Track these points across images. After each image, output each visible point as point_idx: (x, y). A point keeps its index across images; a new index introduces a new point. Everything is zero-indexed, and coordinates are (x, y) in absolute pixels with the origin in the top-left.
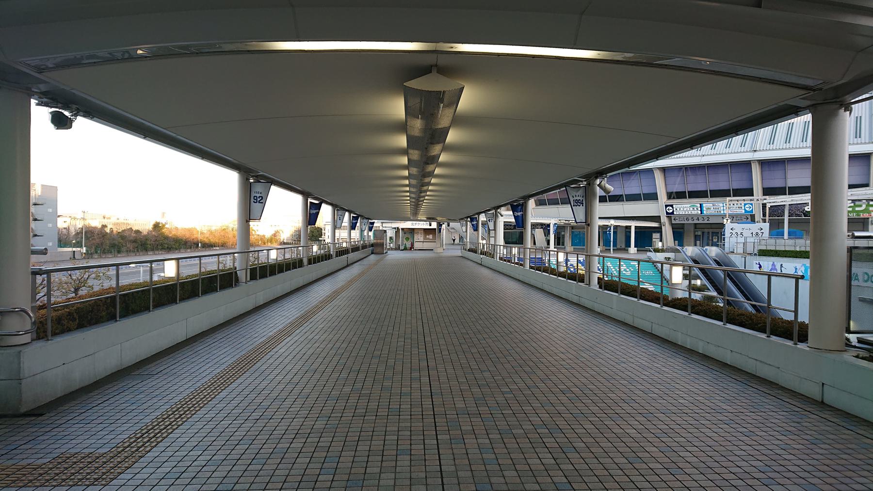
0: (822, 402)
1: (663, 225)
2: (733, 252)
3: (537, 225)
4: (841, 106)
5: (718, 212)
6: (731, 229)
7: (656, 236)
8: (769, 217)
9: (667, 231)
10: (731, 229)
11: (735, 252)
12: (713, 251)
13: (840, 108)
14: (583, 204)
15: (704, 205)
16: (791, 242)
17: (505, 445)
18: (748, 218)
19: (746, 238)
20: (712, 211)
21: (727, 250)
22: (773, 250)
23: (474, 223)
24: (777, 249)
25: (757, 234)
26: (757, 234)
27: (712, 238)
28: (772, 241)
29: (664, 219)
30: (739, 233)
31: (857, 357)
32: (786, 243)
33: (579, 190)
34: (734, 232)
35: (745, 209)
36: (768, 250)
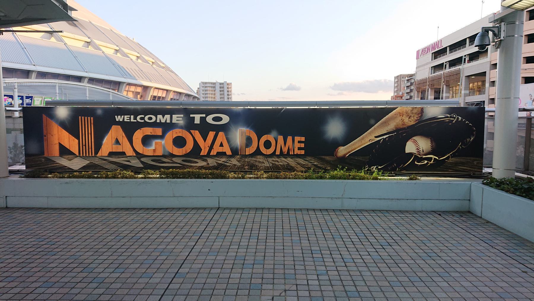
31: (21, 177)
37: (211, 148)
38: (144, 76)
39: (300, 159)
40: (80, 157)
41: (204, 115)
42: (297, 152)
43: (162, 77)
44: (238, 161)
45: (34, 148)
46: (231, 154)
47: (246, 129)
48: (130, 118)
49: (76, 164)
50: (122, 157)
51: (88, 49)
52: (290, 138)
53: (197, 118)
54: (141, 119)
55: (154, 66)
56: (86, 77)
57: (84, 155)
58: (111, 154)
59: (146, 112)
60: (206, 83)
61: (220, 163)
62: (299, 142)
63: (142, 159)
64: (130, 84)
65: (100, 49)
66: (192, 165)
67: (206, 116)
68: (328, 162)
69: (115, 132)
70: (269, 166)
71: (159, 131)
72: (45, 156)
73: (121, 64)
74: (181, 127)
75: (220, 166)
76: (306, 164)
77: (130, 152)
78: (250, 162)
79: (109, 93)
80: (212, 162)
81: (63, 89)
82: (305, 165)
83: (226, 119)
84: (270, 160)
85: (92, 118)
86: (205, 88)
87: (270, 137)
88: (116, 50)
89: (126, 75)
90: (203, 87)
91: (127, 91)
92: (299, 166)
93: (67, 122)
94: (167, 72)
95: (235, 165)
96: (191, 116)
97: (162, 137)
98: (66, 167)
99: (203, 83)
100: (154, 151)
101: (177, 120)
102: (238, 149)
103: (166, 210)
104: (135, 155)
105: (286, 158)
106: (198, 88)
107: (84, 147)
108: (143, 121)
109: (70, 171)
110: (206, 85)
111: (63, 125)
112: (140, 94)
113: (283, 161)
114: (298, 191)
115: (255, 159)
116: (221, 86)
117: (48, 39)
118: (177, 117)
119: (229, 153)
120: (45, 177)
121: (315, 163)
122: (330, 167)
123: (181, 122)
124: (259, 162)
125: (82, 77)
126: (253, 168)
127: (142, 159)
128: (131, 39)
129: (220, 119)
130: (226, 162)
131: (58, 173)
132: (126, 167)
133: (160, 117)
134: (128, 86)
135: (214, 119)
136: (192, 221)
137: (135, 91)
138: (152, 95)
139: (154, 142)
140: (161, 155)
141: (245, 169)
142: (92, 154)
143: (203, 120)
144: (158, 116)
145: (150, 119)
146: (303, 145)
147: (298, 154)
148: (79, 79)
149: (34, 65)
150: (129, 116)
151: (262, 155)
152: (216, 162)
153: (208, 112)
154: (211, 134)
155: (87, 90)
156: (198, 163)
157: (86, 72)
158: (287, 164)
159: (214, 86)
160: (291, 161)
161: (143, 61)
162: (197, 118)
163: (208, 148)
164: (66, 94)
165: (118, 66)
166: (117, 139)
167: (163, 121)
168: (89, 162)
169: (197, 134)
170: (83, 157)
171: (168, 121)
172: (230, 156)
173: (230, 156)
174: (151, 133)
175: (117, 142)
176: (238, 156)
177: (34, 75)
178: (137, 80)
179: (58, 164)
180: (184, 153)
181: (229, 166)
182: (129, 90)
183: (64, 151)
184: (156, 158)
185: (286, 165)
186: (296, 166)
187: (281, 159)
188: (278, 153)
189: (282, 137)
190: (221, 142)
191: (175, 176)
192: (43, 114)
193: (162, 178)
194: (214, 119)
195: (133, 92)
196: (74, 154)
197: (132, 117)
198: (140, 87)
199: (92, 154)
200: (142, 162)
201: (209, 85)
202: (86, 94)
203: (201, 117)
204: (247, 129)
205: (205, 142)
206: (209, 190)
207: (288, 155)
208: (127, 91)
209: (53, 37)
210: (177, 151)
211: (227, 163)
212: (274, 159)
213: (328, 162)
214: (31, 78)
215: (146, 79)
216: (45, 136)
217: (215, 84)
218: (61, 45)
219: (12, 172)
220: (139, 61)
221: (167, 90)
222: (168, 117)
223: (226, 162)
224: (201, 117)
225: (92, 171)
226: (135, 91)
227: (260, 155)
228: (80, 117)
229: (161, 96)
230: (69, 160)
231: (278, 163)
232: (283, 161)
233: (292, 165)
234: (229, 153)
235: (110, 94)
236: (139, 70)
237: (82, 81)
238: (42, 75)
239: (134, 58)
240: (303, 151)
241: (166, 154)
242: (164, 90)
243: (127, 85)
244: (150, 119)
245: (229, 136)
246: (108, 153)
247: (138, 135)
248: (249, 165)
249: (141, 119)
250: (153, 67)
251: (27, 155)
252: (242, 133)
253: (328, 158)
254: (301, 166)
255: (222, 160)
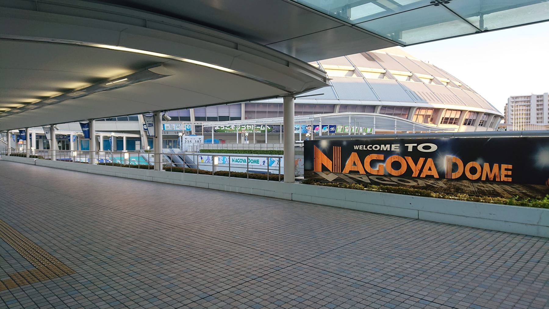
0: (292, 200)
1: (142, 136)
2: (187, 151)
3: (60, 136)
4: (293, 97)
5: (172, 129)
6: (186, 139)
7: (137, 143)
8: (204, 132)
9: (144, 140)
10: (186, 139)
11: (188, 151)
12: (177, 151)
13: (293, 98)
14: (153, 126)
15: (165, 125)
16: (216, 145)
17: (38, 306)
18: (188, 133)
19: (193, 144)
20: (169, 129)
21: (184, 150)
22: (207, 150)
23: (23, 134)
24: (244, 149)
25: (198, 141)
26: (198, 141)
27: (169, 143)
28: (206, 145)
29: (142, 133)
30: (189, 141)
31: (300, 183)
32: (213, 146)
33: (150, 118)
34: (187, 140)
35: (186, 128)
36: (205, 150)
37: (421, 171)
38: (435, 98)
39: (507, 186)
40: (333, 173)
41: (416, 145)
42: (503, 178)
43: (457, 97)
44: (445, 184)
45: (309, 166)
46: (438, 177)
47: (452, 156)
48: (363, 147)
49: (331, 177)
50: (357, 175)
51: (383, 79)
52: (496, 166)
53: (410, 147)
54: (370, 147)
55: (449, 86)
56: (379, 106)
57: (335, 172)
58: (351, 172)
59: (374, 142)
60: (517, 97)
61: (429, 185)
62: (506, 169)
63: (370, 177)
64: (419, 108)
65: (394, 78)
66: (406, 184)
67: (418, 145)
68: (538, 191)
69: (354, 157)
70: (474, 190)
71: (382, 157)
72: (314, 171)
73: (413, 89)
74: (398, 154)
75: (428, 187)
76: (513, 191)
77: (362, 172)
78: (456, 185)
79: (395, 119)
80: (421, 183)
81: (355, 119)
82: (512, 192)
83: (434, 147)
84: (476, 185)
85: (340, 147)
86: (516, 103)
87: (476, 164)
88: (409, 76)
89: (417, 100)
90: (513, 102)
91: (417, 115)
92: (505, 193)
93: (326, 150)
94: (463, 91)
95: (442, 187)
96: (406, 145)
97: (384, 161)
98: (325, 179)
99: (512, 97)
100: (378, 171)
101: (395, 149)
102: (445, 174)
103: (541, 238)
104: (365, 173)
105: (492, 184)
106: (507, 104)
107: (335, 166)
108: (371, 149)
109: (327, 181)
110: (517, 100)
111: (324, 152)
112: (431, 117)
113: (488, 187)
114: (491, 214)
115: (461, 183)
116: (539, 99)
117: (351, 76)
118: (395, 146)
119: (436, 176)
120: (313, 184)
121: (524, 191)
122: (541, 196)
123: (398, 150)
124: (465, 186)
125: (376, 105)
126: (458, 190)
127: (370, 177)
128: (427, 62)
129: (429, 148)
130: (433, 184)
131: (320, 182)
132: (359, 182)
133: (383, 146)
134: (419, 110)
135: (424, 148)
136: (510, 245)
137: (426, 114)
138: (444, 117)
139: (378, 165)
140: (383, 174)
141: (451, 191)
142: (339, 172)
143: (415, 148)
144: (381, 145)
145: (376, 147)
146: (510, 173)
147: (505, 180)
148: (373, 108)
149: (338, 100)
150: (362, 146)
151: (467, 180)
152: (425, 184)
153: (419, 142)
154: (421, 160)
155: (375, 119)
156: (410, 183)
157: (380, 101)
158: (493, 189)
159: (528, 99)
160: (497, 188)
161: (437, 83)
162: (410, 147)
163: (418, 172)
164: (359, 123)
165: (410, 91)
166: (354, 162)
167: (385, 149)
168: (338, 177)
169: (410, 159)
170: (334, 173)
171: (389, 149)
172: (437, 179)
173: (437, 179)
174: (376, 158)
175: (355, 164)
176: (445, 180)
177: (337, 108)
178: (428, 103)
179: (321, 177)
180: (400, 174)
181: (437, 188)
182: (419, 114)
183: (324, 169)
184: (379, 177)
185: (492, 191)
186: (503, 192)
187: (487, 184)
188: (484, 178)
189: (488, 164)
190: (430, 167)
191: (389, 191)
192: (314, 145)
193: (380, 191)
194: (424, 148)
195: (423, 115)
196: (329, 171)
197: (364, 146)
198: (431, 109)
199: (339, 172)
200: (370, 179)
201: (522, 99)
202: (373, 122)
203: (413, 146)
204: (454, 156)
205: (416, 166)
206: (410, 204)
207: (494, 181)
208: (417, 115)
209: (354, 74)
210: (394, 173)
211: (435, 185)
212: (480, 185)
213: (538, 191)
214: (335, 113)
215: (438, 101)
216: (315, 159)
217: (530, 98)
218: (360, 80)
219: (297, 180)
220: (433, 83)
221: (461, 111)
222: (388, 146)
223: (433, 184)
224: (413, 146)
225: (339, 183)
226: (426, 114)
227: (466, 180)
228: (334, 147)
229: (449, 117)
230: (327, 175)
231: (483, 188)
232: (488, 187)
233: (498, 191)
234: (436, 176)
235: (395, 121)
236: (431, 92)
237: (375, 111)
238: (345, 107)
239: (427, 82)
240: (510, 179)
241: (387, 174)
242: (458, 111)
243: (417, 109)
244: (376, 147)
245: (437, 162)
246: (349, 171)
247: (368, 160)
248: (455, 188)
249: (370, 147)
250: (447, 88)
251: (305, 170)
252: (449, 160)
253: (538, 187)
254: (508, 193)
255: (430, 182)
